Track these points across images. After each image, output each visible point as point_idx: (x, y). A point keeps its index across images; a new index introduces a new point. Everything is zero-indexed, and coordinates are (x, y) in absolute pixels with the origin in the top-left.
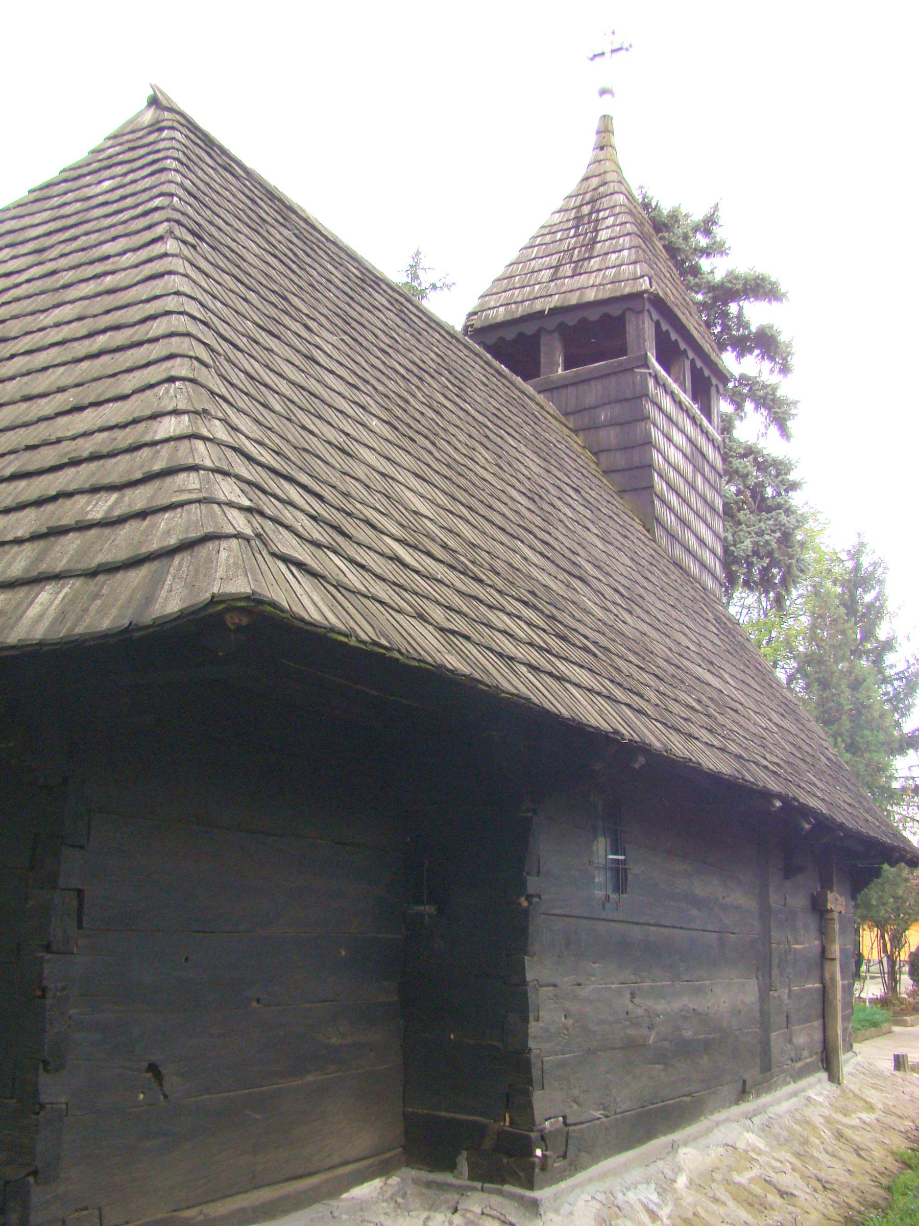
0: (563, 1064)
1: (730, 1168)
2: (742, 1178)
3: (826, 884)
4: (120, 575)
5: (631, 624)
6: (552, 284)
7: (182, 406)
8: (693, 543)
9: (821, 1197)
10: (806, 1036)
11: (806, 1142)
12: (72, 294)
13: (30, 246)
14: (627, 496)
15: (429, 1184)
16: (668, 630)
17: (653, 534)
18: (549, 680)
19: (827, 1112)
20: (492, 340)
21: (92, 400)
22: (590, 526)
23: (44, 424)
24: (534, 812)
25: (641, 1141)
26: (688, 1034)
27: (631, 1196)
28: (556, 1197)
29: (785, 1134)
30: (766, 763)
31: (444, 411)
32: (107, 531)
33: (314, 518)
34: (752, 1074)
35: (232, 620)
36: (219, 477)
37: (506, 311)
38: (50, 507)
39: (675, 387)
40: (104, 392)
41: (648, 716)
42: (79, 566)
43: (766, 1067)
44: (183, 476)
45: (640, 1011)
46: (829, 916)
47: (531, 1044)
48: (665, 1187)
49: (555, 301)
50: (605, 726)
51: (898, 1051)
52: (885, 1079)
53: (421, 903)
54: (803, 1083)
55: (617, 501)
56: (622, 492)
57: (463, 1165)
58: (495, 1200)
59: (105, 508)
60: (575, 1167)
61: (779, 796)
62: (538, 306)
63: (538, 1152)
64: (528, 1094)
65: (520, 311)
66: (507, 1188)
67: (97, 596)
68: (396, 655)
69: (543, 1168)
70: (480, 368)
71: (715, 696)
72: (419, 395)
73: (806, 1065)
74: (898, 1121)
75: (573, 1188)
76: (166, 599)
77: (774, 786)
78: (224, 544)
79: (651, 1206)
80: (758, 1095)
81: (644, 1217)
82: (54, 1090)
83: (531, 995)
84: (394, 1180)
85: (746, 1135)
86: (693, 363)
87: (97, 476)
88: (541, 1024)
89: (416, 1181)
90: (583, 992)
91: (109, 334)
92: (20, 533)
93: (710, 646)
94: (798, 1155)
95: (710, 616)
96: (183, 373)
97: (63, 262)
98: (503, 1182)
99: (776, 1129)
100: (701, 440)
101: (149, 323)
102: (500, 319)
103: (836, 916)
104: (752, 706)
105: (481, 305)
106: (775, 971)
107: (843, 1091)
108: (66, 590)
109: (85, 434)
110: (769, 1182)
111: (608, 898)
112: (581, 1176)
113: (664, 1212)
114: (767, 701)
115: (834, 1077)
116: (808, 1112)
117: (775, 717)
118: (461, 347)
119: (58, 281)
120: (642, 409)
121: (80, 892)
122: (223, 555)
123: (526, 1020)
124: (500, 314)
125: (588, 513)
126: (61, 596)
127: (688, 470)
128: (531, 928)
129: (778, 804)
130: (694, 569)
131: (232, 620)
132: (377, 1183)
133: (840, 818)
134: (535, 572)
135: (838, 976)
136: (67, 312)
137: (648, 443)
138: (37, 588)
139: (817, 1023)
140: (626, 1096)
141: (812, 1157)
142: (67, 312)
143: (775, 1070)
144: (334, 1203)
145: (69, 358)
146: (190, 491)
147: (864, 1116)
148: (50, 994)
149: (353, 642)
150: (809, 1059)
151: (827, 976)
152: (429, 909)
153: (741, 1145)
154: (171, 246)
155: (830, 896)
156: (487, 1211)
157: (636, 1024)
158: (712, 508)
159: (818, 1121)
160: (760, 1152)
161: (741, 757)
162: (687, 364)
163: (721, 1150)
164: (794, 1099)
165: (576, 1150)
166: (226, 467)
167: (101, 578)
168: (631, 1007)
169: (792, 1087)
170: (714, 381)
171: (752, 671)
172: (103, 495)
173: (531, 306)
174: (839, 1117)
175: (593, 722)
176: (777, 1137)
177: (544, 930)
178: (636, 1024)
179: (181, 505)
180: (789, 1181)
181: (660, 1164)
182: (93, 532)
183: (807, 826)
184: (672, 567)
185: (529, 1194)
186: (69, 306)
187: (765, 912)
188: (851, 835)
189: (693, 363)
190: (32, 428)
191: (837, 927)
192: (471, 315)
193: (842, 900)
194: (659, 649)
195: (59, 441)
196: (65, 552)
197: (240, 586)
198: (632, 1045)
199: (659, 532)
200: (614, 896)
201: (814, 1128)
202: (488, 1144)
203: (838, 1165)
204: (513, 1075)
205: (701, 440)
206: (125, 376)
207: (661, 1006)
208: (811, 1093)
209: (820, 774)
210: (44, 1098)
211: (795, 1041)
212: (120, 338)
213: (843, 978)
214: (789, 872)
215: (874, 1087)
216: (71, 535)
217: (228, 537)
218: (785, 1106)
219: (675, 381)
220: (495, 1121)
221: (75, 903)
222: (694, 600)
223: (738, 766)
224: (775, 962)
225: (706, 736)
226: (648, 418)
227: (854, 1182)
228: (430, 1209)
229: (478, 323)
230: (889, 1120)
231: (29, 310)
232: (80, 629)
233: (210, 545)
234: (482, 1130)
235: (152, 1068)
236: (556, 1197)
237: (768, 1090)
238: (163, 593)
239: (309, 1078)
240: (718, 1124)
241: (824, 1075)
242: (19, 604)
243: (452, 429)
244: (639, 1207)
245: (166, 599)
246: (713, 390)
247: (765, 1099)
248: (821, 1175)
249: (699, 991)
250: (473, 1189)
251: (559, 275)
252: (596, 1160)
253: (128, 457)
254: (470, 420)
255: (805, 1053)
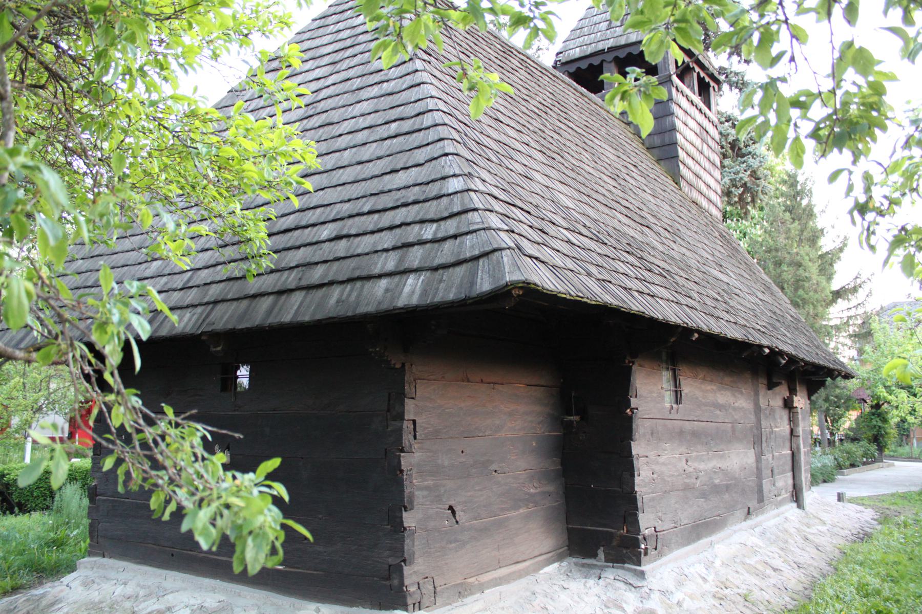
0: (653, 499)
1: (744, 556)
2: (752, 561)
3: (793, 391)
4: (451, 270)
5: (677, 250)
6: (608, 32)
7: (457, 172)
8: (703, 188)
9: (797, 571)
10: (785, 481)
11: (786, 542)
12: (364, 94)
13: (326, 60)
14: (662, 163)
15: (583, 565)
16: (695, 249)
17: (680, 186)
18: (648, 298)
19: (797, 526)
20: (572, 68)
21: (402, 166)
22: (646, 189)
23: (376, 180)
24: (633, 363)
25: (694, 541)
26: (717, 481)
27: (692, 570)
28: (653, 570)
29: (774, 537)
30: (759, 327)
31: (562, 132)
32: (436, 245)
33: (531, 227)
34: (753, 504)
35: (515, 292)
36: (488, 213)
37: (581, 51)
38: (398, 231)
39: (687, 91)
40: (407, 161)
41: (696, 309)
42: (426, 265)
43: (761, 500)
44: (471, 214)
45: (691, 470)
46: (795, 410)
47: (636, 489)
48: (709, 565)
49: (611, 43)
50: (679, 321)
51: (840, 491)
52: (832, 507)
53: (571, 415)
54: (782, 509)
55: (657, 167)
56: (658, 161)
57: (601, 554)
58: (621, 572)
59: (432, 232)
60: (661, 555)
61: (768, 347)
62: (601, 46)
63: (643, 546)
64: (636, 516)
65: (589, 50)
66: (626, 565)
67: (441, 281)
68: (585, 300)
69: (646, 554)
70: (572, 93)
71: (726, 287)
72: (548, 125)
73: (784, 498)
74: (841, 531)
75: (661, 565)
76: (481, 284)
77: (765, 342)
78: (504, 253)
79: (703, 575)
80: (757, 516)
81: (700, 581)
82: (409, 519)
83: (635, 462)
84: (564, 564)
85: (753, 538)
86: (698, 74)
87: (421, 214)
88: (641, 478)
89: (576, 564)
90: (661, 460)
91: (397, 123)
92: (386, 246)
93: (719, 255)
94: (782, 549)
95: (717, 234)
96: (451, 150)
97: (351, 73)
98: (624, 562)
99: (768, 535)
100: (705, 123)
101: (421, 117)
102: (577, 56)
103: (799, 411)
104: (746, 290)
105: (564, 47)
106: (764, 445)
107: (806, 513)
108: (422, 278)
109: (406, 187)
110: (767, 563)
111: (672, 408)
112: (664, 559)
113: (710, 578)
114: (754, 285)
115: (800, 506)
116: (786, 526)
117: (760, 295)
118: (560, 82)
119: (352, 85)
120: (669, 108)
121: (414, 422)
122: (505, 259)
123: (633, 476)
124: (577, 53)
125: (643, 180)
126: (420, 281)
127: (698, 142)
128: (634, 426)
129: (767, 351)
130: (705, 204)
131: (515, 292)
132: (556, 565)
133: (801, 356)
134: (626, 229)
135: (802, 446)
136: (365, 107)
137: (674, 129)
138: (405, 277)
139: (790, 474)
140: (685, 518)
141: (791, 551)
142: (365, 107)
143: (766, 502)
144: (537, 575)
145: (378, 138)
146: (478, 223)
147: (820, 528)
148: (405, 473)
149: (568, 297)
150: (786, 495)
151: (794, 446)
152: (575, 418)
153: (749, 543)
154: (419, 64)
155: (795, 399)
156: (617, 577)
157: (689, 477)
158: (714, 164)
159: (792, 531)
160: (760, 547)
161: (745, 326)
162: (695, 75)
163: (738, 546)
164: (778, 519)
165: (660, 545)
166: (490, 208)
167: (441, 271)
168: (686, 467)
169: (776, 511)
170: (712, 84)
171: (743, 266)
172: (428, 225)
173: (596, 47)
174: (805, 528)
175: (673, 320)
176: (769, 539)
177: (641, 427)
178: (689, 476)
179: (475, 231)
180: (778, 563)
181: (705, 553)
182: (428, 245)
183: (784, 362)
184: (692, 205)
185: (638, 568)
186: (365, 103)
187: (758, 409)
188: (807, 363)
189: (698, 74)
190: (369, 181)
191: (800, 416)
192: (558, 54)
193: (802, 401)
194: (692, 263)
195: (390, 191)
196: (416, 256)
197: (516, 277)
198: (687, 488)
199: (683, 183)
200: (675, 406)
201: (790, 534)
202: (615, 543)
203: (806, 555)
204: (626, 505)
205: (705, 123)
206: (416, 151)
207: (702, 466)
208: (787, 515)
209: (788, 327)
210: (406, 525)
211: (777, 484)
212: (406, 126)
213: (804, 447)
214: (771, 386)
215: (826, 511)
216: (416, 247)
217: (504, 249)
218: (772, 522)
219: (688, 87)
220: (618, 530)
221: (412, 427)
222: (706, 225)
223: (745, 332)
224: (764, 439)
225: (727, 316)
226: (673, 114)
227: (816, 564)
228: (586, 577)
229: (563, 58)
230: (835, 530)
231: (340, 104)
232: (438, 299)
233: (497, 254)
234: (611, 535)
235: (451, 508)
236: (653, 570)
237: (763, 513)
238: (479, 280)
239: (521, 511)
240: (735, 532)
241: (795, 505)
242: (397, 286)
243: (568, 144)
244: (696, 575)
245: (481, 284)
246: (711, 89)
247: (761, 518)
248: (796, 560)
249: (722, 457)
250: (608, 567)
251: (612, 25)
252: (671, 550)
253: (435, 202)
254: (574, 133)
255: (783, 492)
